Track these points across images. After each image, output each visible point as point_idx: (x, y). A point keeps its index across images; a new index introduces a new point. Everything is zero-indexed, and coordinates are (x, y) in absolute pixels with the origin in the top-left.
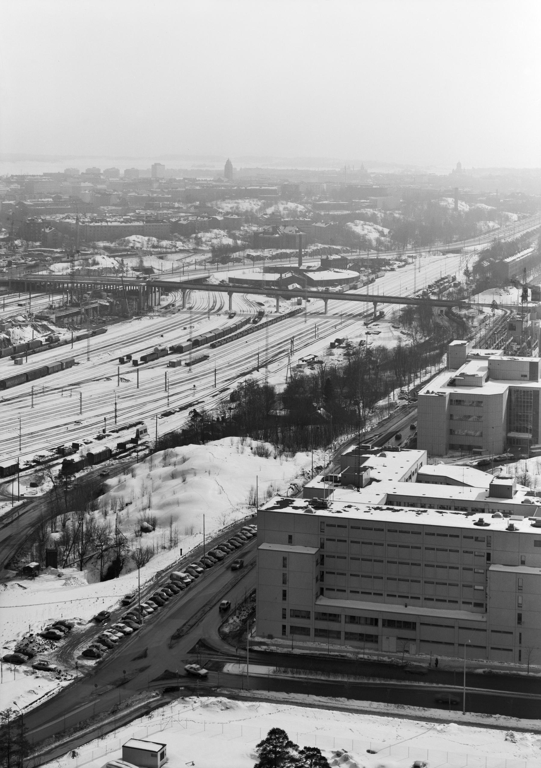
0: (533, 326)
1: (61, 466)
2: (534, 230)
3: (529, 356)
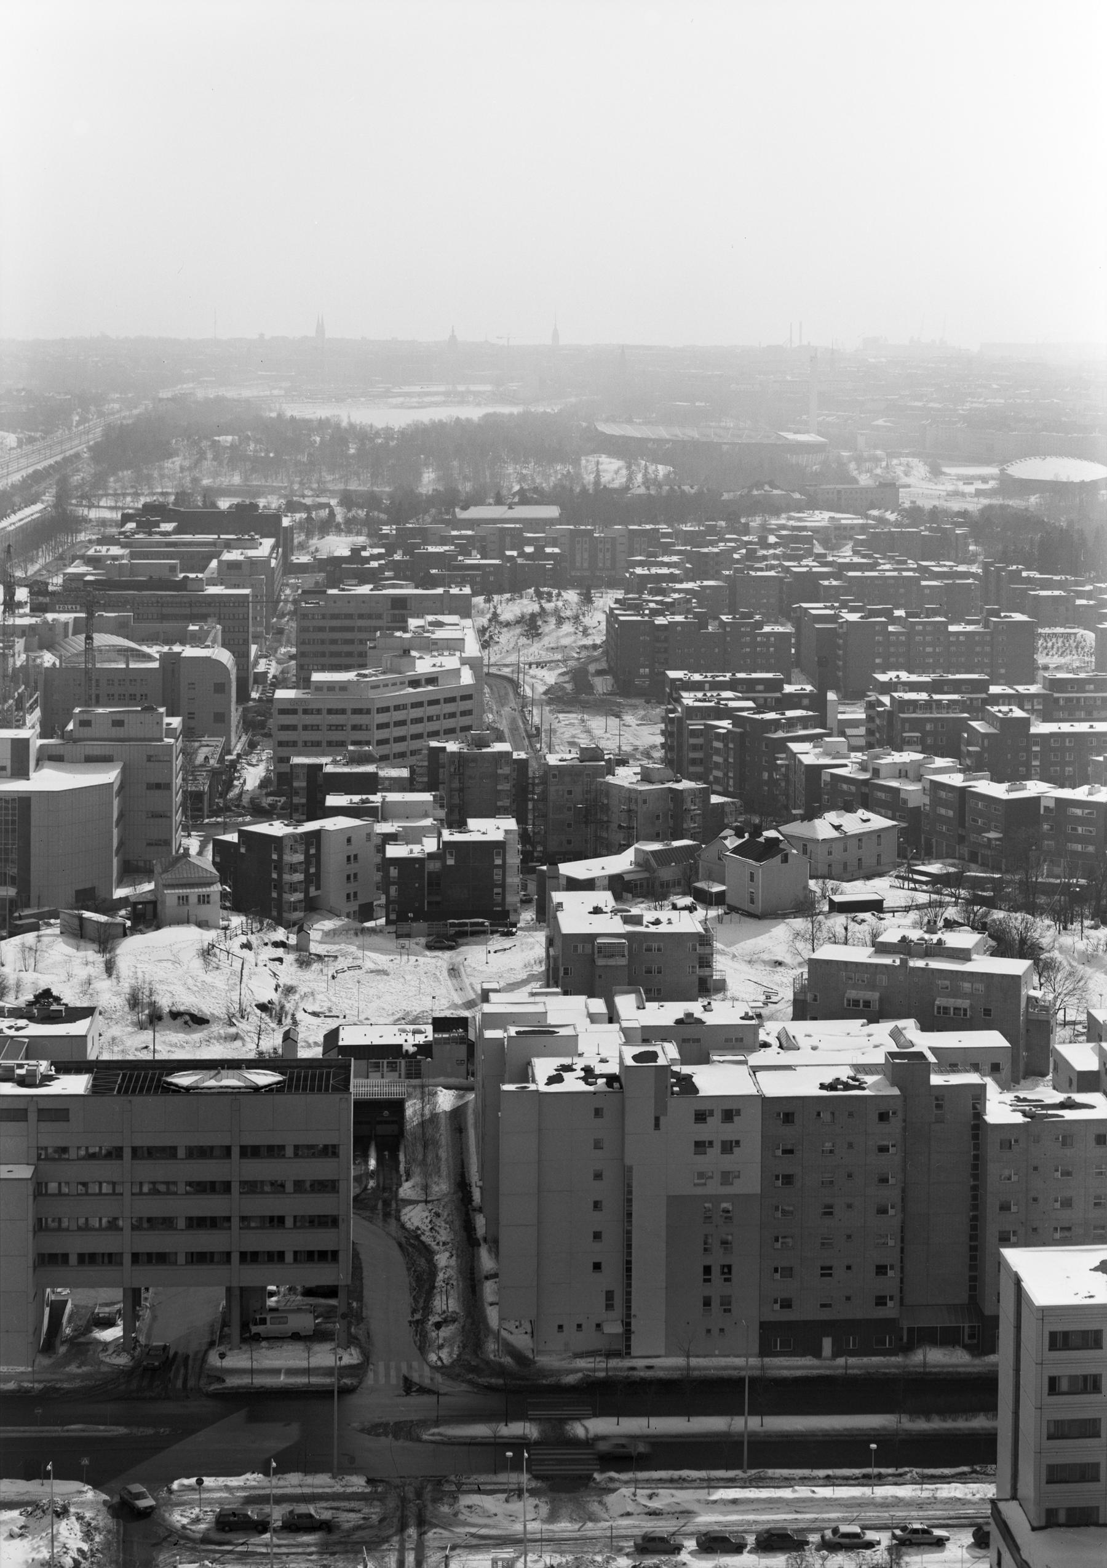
0: (31, 662)
1: (666, 1044)
2: (51, 466)
3: (18, 727)
